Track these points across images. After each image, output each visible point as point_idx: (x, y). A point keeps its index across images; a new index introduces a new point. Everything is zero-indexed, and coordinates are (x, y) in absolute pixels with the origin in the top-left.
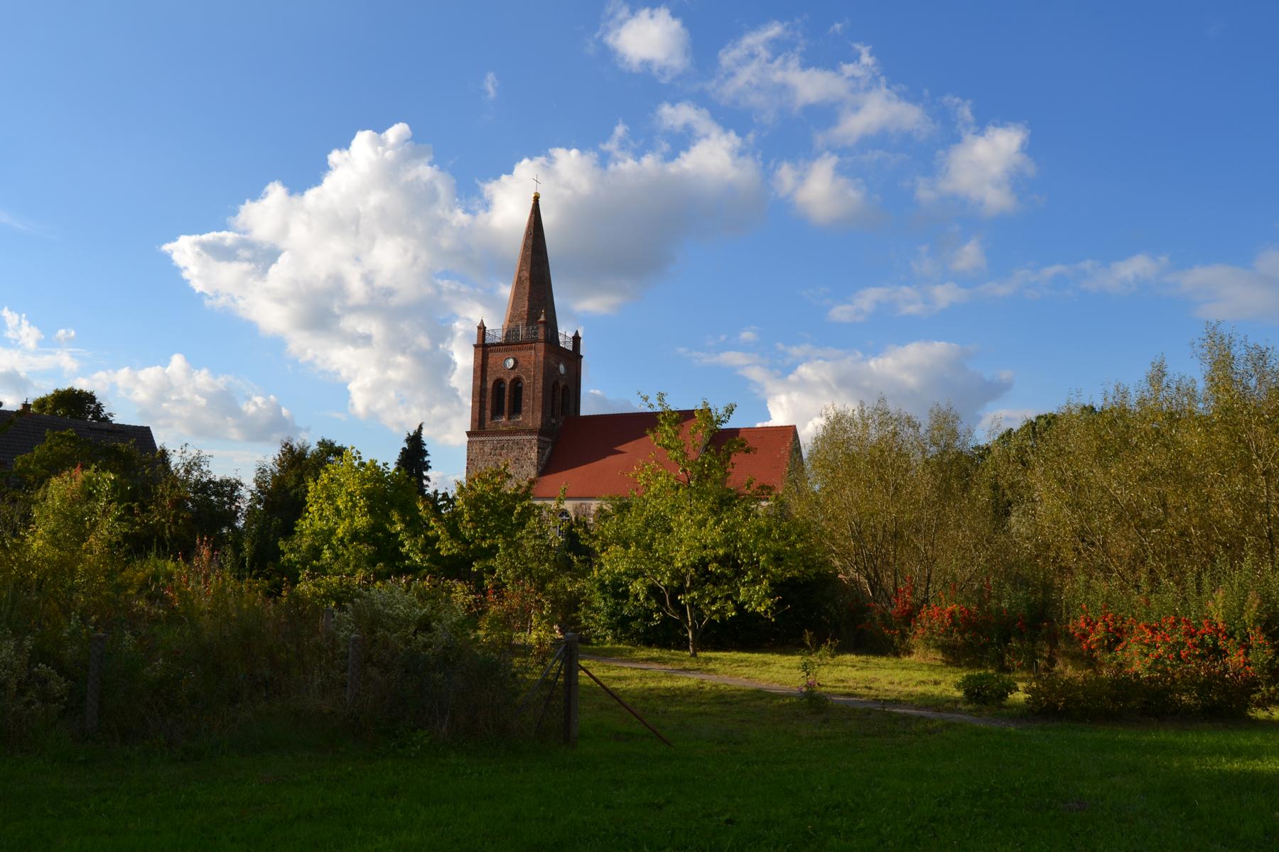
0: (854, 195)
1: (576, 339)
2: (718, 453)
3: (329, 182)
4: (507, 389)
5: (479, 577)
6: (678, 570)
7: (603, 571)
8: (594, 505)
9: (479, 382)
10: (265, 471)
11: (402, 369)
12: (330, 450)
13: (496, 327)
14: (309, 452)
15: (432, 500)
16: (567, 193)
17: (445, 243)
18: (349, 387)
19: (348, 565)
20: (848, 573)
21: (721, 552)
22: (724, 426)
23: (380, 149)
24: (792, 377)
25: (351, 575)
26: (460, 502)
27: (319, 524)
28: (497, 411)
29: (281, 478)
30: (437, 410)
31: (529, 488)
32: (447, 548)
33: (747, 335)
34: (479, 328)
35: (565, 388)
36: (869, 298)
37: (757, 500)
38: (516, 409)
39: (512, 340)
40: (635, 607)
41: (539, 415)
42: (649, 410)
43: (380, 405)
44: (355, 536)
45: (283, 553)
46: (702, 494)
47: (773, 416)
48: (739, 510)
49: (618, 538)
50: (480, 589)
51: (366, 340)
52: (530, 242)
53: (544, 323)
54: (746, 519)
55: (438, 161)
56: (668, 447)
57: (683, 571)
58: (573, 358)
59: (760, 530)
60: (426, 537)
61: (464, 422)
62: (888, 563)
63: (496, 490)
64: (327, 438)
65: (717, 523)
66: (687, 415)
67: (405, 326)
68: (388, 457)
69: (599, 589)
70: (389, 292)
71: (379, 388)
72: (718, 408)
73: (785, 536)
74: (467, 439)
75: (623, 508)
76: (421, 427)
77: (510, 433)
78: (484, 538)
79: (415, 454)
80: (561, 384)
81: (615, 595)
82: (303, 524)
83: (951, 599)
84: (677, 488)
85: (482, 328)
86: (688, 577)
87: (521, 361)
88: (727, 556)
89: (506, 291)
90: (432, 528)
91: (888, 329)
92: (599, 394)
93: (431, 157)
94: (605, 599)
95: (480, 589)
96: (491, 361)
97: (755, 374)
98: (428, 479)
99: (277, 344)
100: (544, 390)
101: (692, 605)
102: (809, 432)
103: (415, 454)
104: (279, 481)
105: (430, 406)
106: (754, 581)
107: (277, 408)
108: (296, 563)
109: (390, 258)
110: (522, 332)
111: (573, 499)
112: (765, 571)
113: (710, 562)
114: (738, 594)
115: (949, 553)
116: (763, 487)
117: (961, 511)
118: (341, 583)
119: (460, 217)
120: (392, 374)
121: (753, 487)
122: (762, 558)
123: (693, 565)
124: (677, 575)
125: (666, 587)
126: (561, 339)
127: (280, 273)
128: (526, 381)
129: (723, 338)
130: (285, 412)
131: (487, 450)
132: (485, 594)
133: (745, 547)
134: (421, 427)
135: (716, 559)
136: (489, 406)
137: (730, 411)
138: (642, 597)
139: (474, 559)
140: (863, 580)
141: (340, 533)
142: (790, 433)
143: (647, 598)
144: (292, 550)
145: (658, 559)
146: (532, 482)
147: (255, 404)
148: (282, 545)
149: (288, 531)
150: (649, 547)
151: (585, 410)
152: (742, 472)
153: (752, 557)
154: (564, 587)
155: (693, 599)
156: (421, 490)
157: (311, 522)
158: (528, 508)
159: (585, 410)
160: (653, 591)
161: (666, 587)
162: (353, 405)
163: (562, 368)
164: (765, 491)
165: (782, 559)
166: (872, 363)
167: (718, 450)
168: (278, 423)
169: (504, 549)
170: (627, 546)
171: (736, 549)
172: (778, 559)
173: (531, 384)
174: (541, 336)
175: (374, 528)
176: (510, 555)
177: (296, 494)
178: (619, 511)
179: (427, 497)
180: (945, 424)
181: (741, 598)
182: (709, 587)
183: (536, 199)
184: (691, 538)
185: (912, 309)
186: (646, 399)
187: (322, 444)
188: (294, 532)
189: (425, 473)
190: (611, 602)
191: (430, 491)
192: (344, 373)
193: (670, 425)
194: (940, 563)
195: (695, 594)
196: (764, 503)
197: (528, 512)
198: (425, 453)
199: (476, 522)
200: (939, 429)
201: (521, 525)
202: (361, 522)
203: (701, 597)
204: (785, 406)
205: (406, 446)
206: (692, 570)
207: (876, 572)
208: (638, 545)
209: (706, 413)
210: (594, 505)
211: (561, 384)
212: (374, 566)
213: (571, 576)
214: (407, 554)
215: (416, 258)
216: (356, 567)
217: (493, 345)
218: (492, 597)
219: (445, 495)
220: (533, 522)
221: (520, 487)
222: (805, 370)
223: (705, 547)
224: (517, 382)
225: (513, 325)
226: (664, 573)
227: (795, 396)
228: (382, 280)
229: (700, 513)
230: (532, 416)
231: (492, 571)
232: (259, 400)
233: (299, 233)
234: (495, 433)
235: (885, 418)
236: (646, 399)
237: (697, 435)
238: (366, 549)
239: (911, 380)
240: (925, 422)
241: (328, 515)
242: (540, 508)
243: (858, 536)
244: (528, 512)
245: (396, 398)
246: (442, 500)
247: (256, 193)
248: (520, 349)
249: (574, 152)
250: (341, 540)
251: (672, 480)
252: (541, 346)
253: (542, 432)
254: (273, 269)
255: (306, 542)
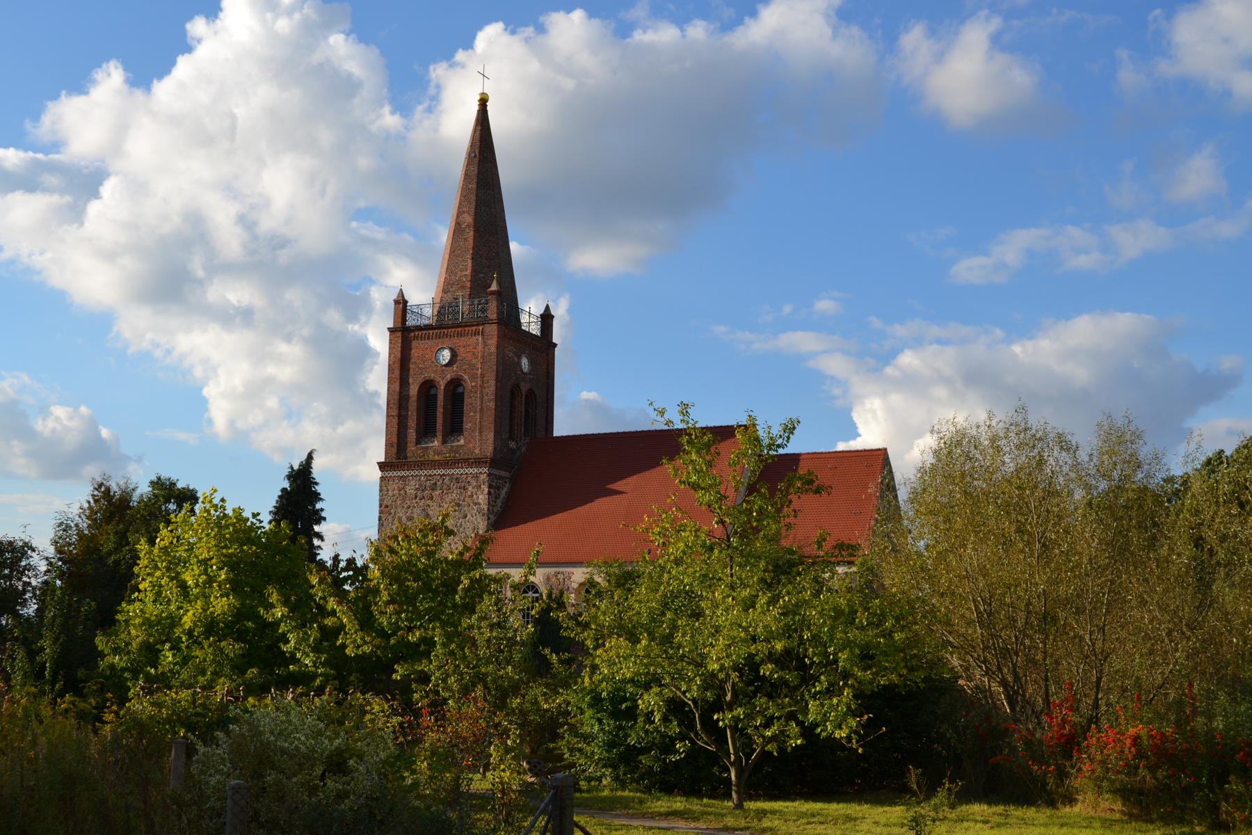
0: (1022, 78)
1: (547, 319)
2: (772, 495)
3: (184, 67)
4: (441, 397)
5: (404, 688)
6: (713, 675)
7: (597, 678)
8: (579, 575)
9: (397, 386)
10: (68, 527)
11: (289, 362)
12: (172, 496)
13: (423, 295)
14: (136, 497)
15: (333, 575)
16: (569, 84)
17: (364, 162)
18: (205, 392)
19: (203, 673)
20: (973, 678)
21: (779, 646)
22: (781, 451)
23: (269, 15)
24: (889, 370)
25: (209, 687)
26: (375, 572)
27: (152, 610)
28: (426, 431)
29: (92, 538)
30: (349, 427)
31: (481, 550)
32: (355, 643)
33: (825, 305)
34: (397, 302)
35: (531, 392)
36: (1014, 247)
37: (830, 564)
38: (455, 427)
39: (447, 320)
40: (647, 732)
41: (491, 436)
42: (666, 428)
43: (255, 418)
44: (210, 627)
45: (102, 655)
46: (749, 558)
47: (861, 430)
48: (806, 582)
49: (621, 627)
50: (408, 707)
51: (245, 316)
52: (474, 169)
53: (498, 293)
54: (817, 594)
55: (361, 32)
56: (696, 487)
57: (722, 676)
58: (542, 346)
59: (839, 612)
60: (322, 628)
61: (378, 451)
62: (1035, 662)
63: (429, 555)
64: (165, 475)
65: (773, 601)
66: (724, 433)
67: (294, 296)
68: (258, 501)
69: (591, 706)
70: (278, 242)
71: (255, 391)
72: (769, 425)
73: (877, 621)
74: (378, 474)
75: (626, 580)
76: (310, 457)
77: (446, 464)
78: (410, 629)
79: (300, 499)
80: (524, 388)
81: (616, 714)
82: (131, 610)
83: (1134, 717)
84: (711, 549)
85: (401, 304)
86: (729, 686)
87: (461, 352)
88: (787, 652)
89: (443, 236)
90: (333, 613)
91: (1046, 294)
92: (577, 409)
93: (347, 26)
94: (600, 721)
95: (408, 707)
96: (415, 353)
97: (835, 365)
98: (320, 537)
99: (99, 323)
100: (498, 398)
101: (735, 729)
102: (911, 458)
103: (300, 499)
104: (88, 544)
105: (336, 420)
106: (830, 692)
107: (92, 425)
108: (124, 670)
109: (286, 189)
110: (464, 307)
111: (549, 565)
112: (846, 675)
113: (762, 661)
114: (805, 711)
115: (1129, 646)
116: (841, 546)
117: (1146, 580)
118: (194, 701)
119: (390, 120)
120: (271, 370)
121: (827, 546)
122: (843, 656)
123: (736, 668)
124: (711, 681)
125: (694, 700)
126: (524, 319)
127: (107, 210)
128: (469, 384)
129: (788, 309)
130: (105, 433)
131: (410, 490)
132: (417, 713)
133: (815, 639)
134: (310, 457)
135: (771, 657)
136: (412, 423)
137: (790, 429)
138: (657, 717)
139: (397, 660)
140: (996, 688)
141: (187, 621)
142: (879, 459)
143: (665, 719)
144: (116, 651)
145: (682, 658)
146: (484, 541)
147: (57, 419)
148: (100, 642)
149: (106, 620)
150: (668, 639)
151: (563, 425)
152: (807, 523)
153: (826, 655)
154: (536, 703)
155: (736, 719)
156: (312, 553)
157: (136, 612)
158: (478, 581)
159: (563, 425)
160: (675, 707)
161: (694, 700)
162: (210, 422)
163: (525, 363)
164: (846, 551)
165: (872, 657)
166: (1017, 349)
167: (773, 491)
168: (93, 448)
169: (443, 645)
170: (634, 640)
171: (801, 641)
172: (866, 657)
173: (474, 386)
174: (492, 313)
175: (240, 614)
176: (452, 653)
177: (117, 563)
178: (618, 585)
179: (321, 564)
180: (1119, 441)
181: (811, 717)
182: (760, 701)
183: (483, 102)
184: (733, 624)
185: (1083, 262)
186: (662, 413)
187: (158, 484)
188: (114, 622)
189: (317, 528)
190: (609, 724)
191: (325, 555)
192: (198, 372)
193: (698, 452)
194: (1117, 663)
195: (740, 711)
196: (840, 570)
197: (480, 588)
198: (316, 497)
199: (401, 604)
200: (1111, 453)
201: (470, 609)
202: (221, 605)
203: (750, 717)
204: (880, 414)
205: (286, 485)
206: (734, 676)
207: (1016, 675)
208: (652, 637)
209: (748, 429)
210: (579, 575)
211: (524, 388)
212: (244, 673)
213: (547, 686)
214: (293, 655)
215: (323, 193)
216: (217, 674)
217: (419, 328)
218: (428, 720)
219: (351, 562)
220: (487, 604)
221: (466, 549)
222: (908, 359)
223: (754, 639)
224: (455, 383)
225: (449, 297)
226: (691, 680)
227: (896, 399)
228: (267, 224)
229: (746, 586)
230: (479, 437)
231: (424, 678)
232: (60, 412)
233: (144, 146)
234: (421, 465)
235: (1030, 440)
236: (662, 413)
237: (735, 469)
238: (231, 648)
239: (1080, 374)
240: (1087, 441)
241: (171, 592)
242: (497, 581)
243: (987, 619)
244: (480, 588)
245: (276, 410)
246: (344, 570)
247: (79, 84)
248: (460, 335)
249: (578, 15)
250: (190, 633)
251: (703, 536)
252: (492, 330)
253: (494, 462)
254: (94, 208)
255: (137, 636)
